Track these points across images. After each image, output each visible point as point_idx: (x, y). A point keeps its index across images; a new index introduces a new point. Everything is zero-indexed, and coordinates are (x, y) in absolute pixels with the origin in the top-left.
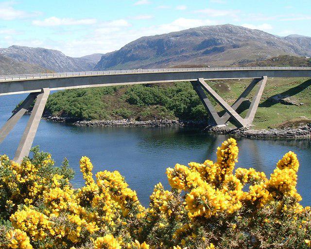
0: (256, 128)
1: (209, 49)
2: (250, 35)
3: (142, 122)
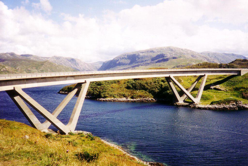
0: (203, 104)
1: (160, 59)
2: (182, 51)
3: (135, 100)
